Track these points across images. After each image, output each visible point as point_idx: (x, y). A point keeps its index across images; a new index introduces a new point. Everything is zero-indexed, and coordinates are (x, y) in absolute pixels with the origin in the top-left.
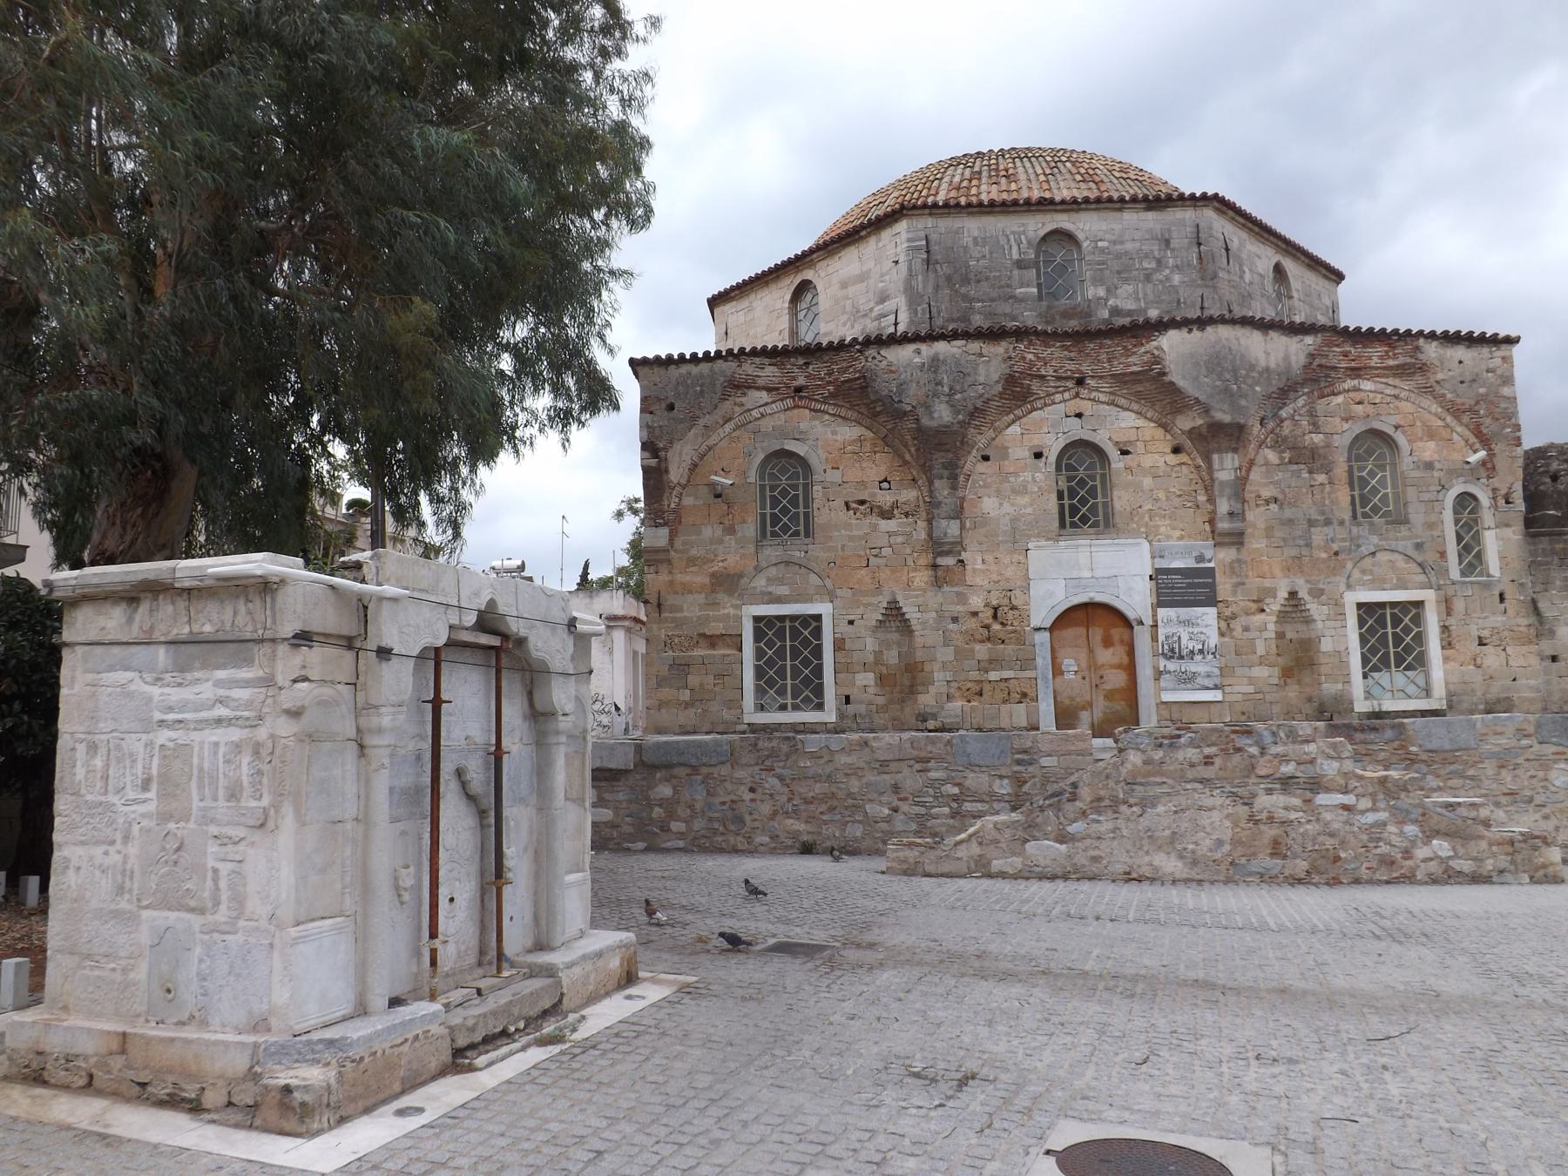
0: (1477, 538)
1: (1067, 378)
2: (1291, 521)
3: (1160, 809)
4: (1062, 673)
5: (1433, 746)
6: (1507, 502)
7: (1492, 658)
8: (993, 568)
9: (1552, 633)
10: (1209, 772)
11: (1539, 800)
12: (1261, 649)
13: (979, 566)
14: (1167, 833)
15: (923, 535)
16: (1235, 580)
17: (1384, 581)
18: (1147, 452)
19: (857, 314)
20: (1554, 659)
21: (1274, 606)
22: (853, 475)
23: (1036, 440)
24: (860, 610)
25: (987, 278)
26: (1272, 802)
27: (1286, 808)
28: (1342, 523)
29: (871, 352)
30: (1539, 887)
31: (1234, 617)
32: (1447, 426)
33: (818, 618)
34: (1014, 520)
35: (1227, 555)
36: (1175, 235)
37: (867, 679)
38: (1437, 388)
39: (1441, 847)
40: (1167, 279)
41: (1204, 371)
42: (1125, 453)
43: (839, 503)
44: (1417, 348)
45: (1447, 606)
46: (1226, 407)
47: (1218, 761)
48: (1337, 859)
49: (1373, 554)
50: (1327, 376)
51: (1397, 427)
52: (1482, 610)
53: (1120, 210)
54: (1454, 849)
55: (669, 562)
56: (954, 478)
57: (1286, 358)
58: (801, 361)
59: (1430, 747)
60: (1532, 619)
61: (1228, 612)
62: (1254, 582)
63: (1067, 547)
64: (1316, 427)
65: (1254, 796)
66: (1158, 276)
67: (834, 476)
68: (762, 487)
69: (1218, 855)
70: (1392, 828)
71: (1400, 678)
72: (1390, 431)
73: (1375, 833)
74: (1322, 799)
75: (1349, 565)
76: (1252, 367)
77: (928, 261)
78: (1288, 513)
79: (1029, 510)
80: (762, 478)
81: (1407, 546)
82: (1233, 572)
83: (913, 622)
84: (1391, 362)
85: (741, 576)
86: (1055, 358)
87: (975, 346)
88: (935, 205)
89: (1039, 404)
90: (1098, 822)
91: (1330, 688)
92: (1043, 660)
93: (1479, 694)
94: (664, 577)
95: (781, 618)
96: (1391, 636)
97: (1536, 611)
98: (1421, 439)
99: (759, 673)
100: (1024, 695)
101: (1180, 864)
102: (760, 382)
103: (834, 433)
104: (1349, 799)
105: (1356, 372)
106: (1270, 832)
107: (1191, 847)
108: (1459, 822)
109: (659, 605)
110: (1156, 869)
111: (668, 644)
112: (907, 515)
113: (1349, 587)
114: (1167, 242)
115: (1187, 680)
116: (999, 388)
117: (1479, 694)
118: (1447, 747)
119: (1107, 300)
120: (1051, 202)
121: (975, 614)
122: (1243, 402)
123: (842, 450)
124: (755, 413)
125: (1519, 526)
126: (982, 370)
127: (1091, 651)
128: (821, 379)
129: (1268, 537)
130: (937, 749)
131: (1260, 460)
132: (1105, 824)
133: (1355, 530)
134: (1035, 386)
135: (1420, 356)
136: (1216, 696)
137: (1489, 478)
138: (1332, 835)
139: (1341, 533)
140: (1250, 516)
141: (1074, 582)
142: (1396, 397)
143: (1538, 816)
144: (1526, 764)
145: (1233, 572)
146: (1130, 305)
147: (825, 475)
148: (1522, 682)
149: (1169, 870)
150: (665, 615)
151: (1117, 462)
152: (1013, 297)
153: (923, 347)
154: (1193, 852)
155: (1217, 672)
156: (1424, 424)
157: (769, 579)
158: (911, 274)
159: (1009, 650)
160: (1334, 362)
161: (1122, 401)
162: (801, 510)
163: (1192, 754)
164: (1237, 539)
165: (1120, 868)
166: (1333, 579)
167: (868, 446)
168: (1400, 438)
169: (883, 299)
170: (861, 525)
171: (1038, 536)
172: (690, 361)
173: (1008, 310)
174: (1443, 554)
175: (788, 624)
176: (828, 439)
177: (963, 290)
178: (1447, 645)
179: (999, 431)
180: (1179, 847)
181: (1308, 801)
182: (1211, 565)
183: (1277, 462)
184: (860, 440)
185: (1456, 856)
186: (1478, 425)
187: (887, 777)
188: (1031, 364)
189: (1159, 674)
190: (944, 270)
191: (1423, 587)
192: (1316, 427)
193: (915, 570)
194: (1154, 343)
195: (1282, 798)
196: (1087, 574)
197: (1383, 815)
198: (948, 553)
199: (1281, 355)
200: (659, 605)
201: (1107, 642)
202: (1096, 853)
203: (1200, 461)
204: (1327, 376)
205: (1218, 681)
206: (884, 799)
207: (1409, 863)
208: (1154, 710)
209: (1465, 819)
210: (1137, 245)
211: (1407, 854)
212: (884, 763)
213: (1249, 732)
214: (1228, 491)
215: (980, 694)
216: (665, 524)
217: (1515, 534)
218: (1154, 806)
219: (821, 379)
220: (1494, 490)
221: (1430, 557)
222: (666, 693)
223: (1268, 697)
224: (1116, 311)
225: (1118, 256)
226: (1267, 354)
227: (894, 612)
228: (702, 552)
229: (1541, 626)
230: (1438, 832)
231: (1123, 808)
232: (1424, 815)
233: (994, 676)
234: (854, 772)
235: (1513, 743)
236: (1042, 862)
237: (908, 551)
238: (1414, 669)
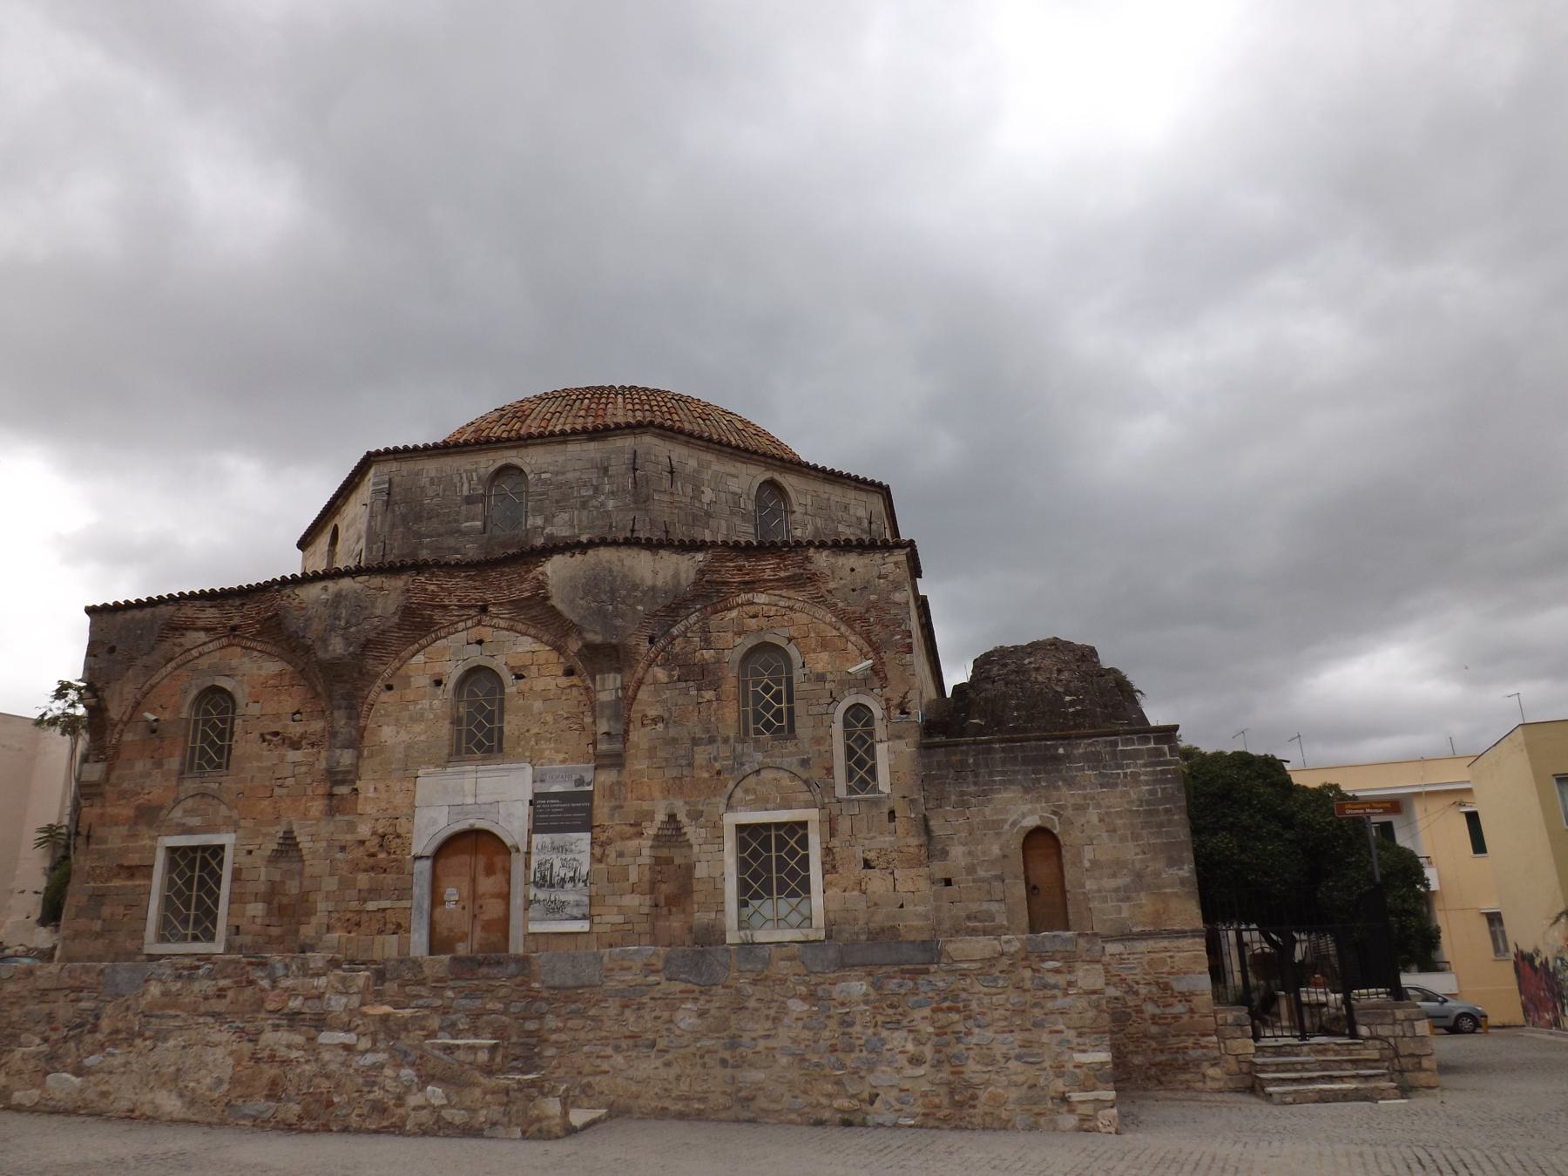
0: (871, 751)
2: (674, 740)
3: (171, 1043)
4: (444, 903)
5: (557, 982)
6: (903, 712)
7: (878, 883)
9: (944, 854)
10: (220, 1006)
11: (662, 1044)
12: (633, 877)
14: (173, 1069)
16: (614, 803)
18: (540, 675)
20: (948, 882)
21: (651, 830)
23: (437, 668)
24: (259, 841)
25: (438, 515)
26: (277, 1039)
27: (289, 1046)
28: (726, 740)
29: (287, 591)
30: (533, 1144)
31: (610, 841)
32: (842, 636)
33: (222, 847)
34: (409, 747)
35: (607, 777)
36: (613, 462)
38: (829, 597)
39: (435, 1094)
40: (602, 504)
41: (581, 594)
42: (519, 677)
43: (256, 734)
44: (808, 559)
47: (230, 994)
48: (330, 1104)
49: (758, 772)
50: (718, 591)
52: (869, 830)
53: (565, 442)
54: (447, 1097)
55: (101, 795)
57: (676, 576)
58: (238, 603)
59: (551, 983)
60: (923, 839)
61: (603, 837)
62: (632, 805)
63: (454, 773)
64: (707, 643)
65: (260, 1032)
69: (216, 1095)
70: (388, 1072)
71: (784, 905)
72: (782, 643)
73: (371, 1077)
74: (326, 1037)
75: (731, 785)
76: (635, 587)
77: (387, 503)
78: (672, 732)
79: (423, 738)
81: (792, 762)
82: (612, 795)
83: (305, 852)
84: (783, 574)
85: (161, 808)
86: (459, 588)
87: (377, 581)
88: (552, 434)
90: (113, 1055)
91: (702, 917)
92: (421, 890)
93: (861, 922)
94: (97, 810)
96: (771, 860)
97: (927, 830)
98: (814, 651)
99: (167, 903)
100: (399, 926)
101: (179, 1103)
102: (200, 623)
103: (260, 668)
104: (350, 1038)
105: (750, 586)
106: (271, 1071)
107: (192, 1084)
108: (456, 1066)
109: (88, 837)
110: (157, 1107)
112: (313, 745)
114: (606, 470)
115: (555, 909)
116: (396, 619)
117: (861, 922)
118: (570, 983)
120: (607, 428)
121: (362, 842)
122: (619, 622)
124: (195, 653)
125: (914, 737)
126: (380, 603)
127: (474, 880)
129: (651, 758)
130: (89, 979)
131: (649, 678)
132: (119, 1057)
133: (739, 747)
134: (437, 615)
135: (809, 566)
136: (583, 926)
137: (882, 688)
138: (327, 1077)
139: (725, 751)
140: (634, 736)
141: (458, 809)
142: (791, 609)
143: (658, 1063)
144: (652, 1004)
145: (612, 795)
147: (248, 708)
148: (909, 908)
149: (169, 1109)
150: (92, 846)
152: (459, 531)
154: (193, 1090)
155: (586, 900)
157: (185, 811)
159: (389, 879)
160: (727, 577)
161: (520, 627)
163: (207, 986)
164: (616, 761)
165: (124, 1104)
166: (713, 800)
168: (793, 651)
171: (429, 763)
174: (829, 771)
175: (199, 855)
176: (251, 673)
177: (415, 527)
178: (829, 868)
180: (181, 1085)
181: (311, 1039)
182: (590, 788)
184: (281, 674)
185: (449, 1105)
186: (869, 633)
187: (43, 1006)
188: (434, 595)
189: (528, 903)
190: (400, 509)
191: (808, 805)
192: (707, 643)
193: (313, 799)
195: (286, 1035)
196: (470, 800)
197: (382, 1057)
198: (343, 782)
199: (671, 573)
200: (88, 837)
201: (490, 871)
202: (104, 1088)
204: (718, 591)
205: (586, 910)
206: (39, 1028)
207: (401, 1111)
208: (521, 941)
209: (462, 1064)
210: (577, 474)
211: (400, 1100)
212: (45, 992)
213: (263, 964)
214: (607, 712)
215: (358, 924)
217: (907, 748)
218: (165, 1040)
220: (888, 700)
221: (816, 773)
223: (637, 928)
224: (551, 537)
225: (559, 486)
226: (656, 573)
227: (289, 845)
229: (932, 849)
230: (433, 1077)
231: (138, 1041)
232: (421, 1057)
233: (371, 906)
234: (18, 1000)
235: (640, 979)
236: (58, 1095)
238: (761, 897)
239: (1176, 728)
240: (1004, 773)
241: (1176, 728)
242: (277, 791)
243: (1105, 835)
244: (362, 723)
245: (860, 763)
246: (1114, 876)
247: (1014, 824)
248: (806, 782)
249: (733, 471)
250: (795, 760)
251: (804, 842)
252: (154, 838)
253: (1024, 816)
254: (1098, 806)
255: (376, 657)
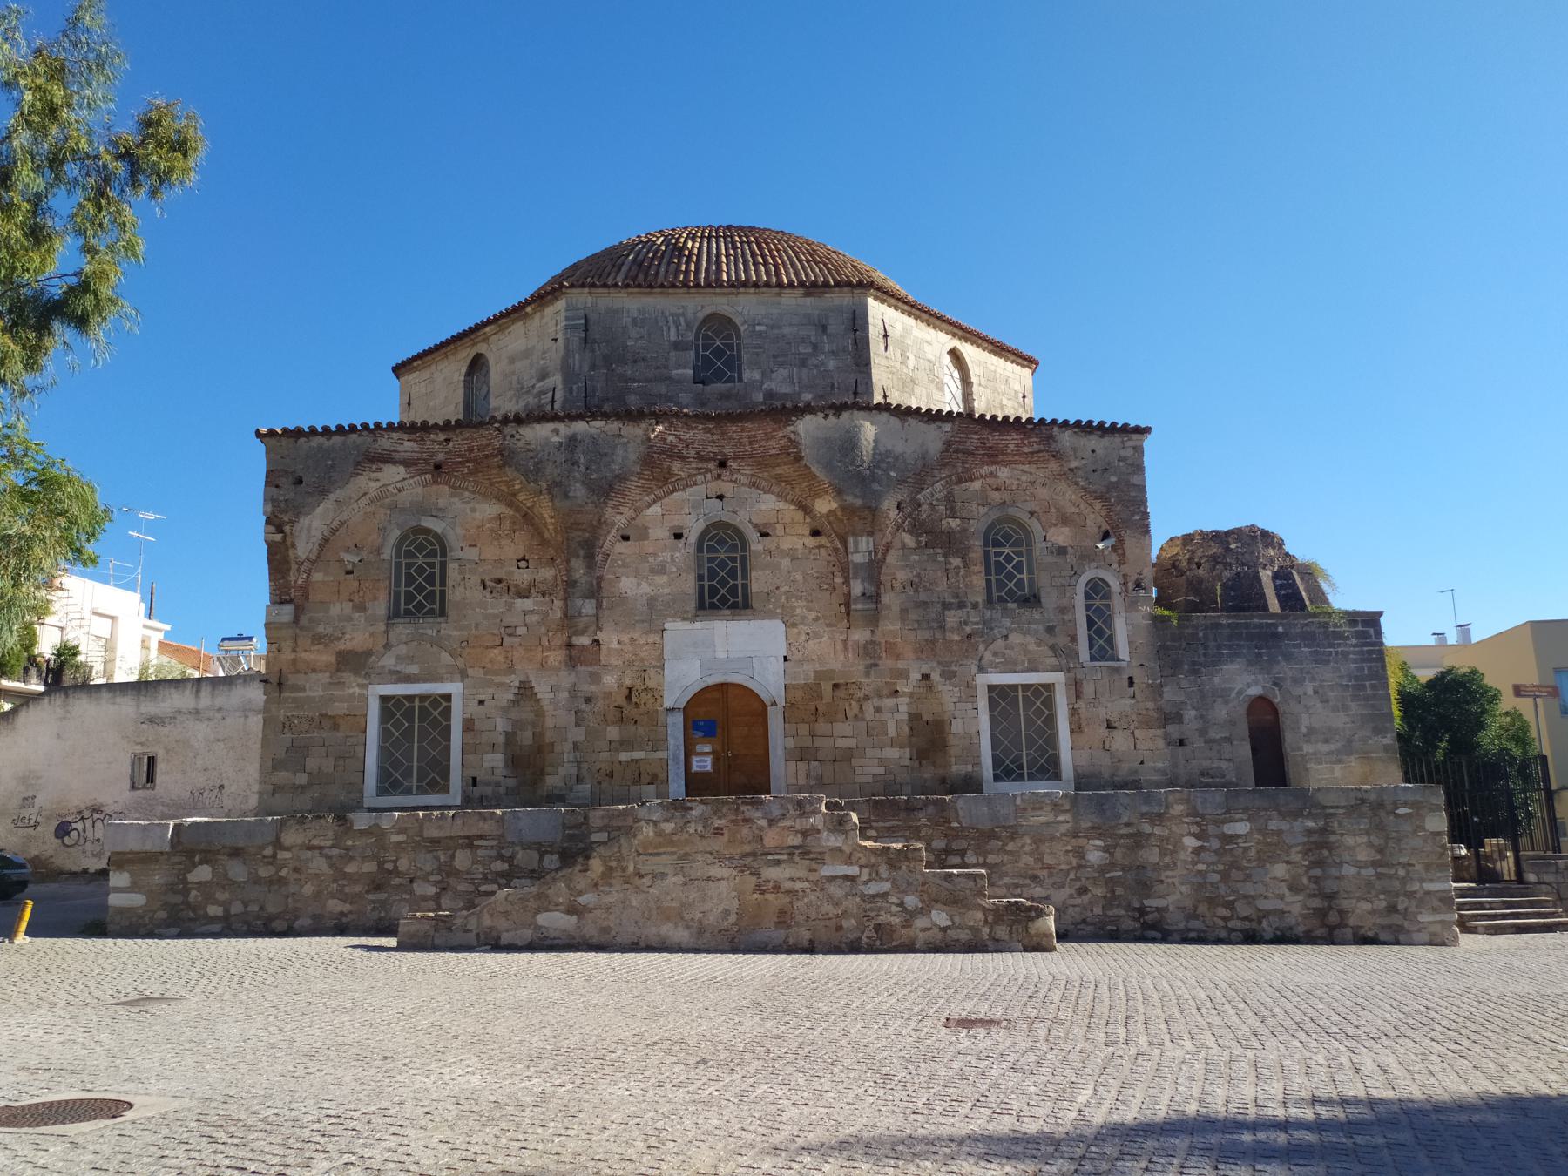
0: (1109, 622)
1: (708, 460)
2: (925, 604)
7: (1120, 742)
8: (628, 648)
13: (615, 645)
15: (559, 614)
17: (1015, 663)
19: (522, 390)
22: (490, 553)
23: (676, 521)
28: (975, 606)
29: (509, 429)
33: (448, 697)
37: (496, 760)
42: (764, 535)
43: (476, 580)
44: (1051, 437)
45: (1076, 688)
46: (857, 491)
51: (1032, 514)
54: (951, 918)
56: (590, 558)
66: (812, 361)
67: (472, 554)
68: (398, 565)
72: (1024, 517)
75: (982, 648)
78: (923, 596)
79: (666, 591)
80: (398, 555)
82: (867, 654)
83: (545, 703)
84: (1026, 450)
89: (680, 484)
95: (410, 698)
103: (473, 510)
109: (280, 684)
111: (286, 725)
113: (981, 670)
114: (824, 328)
119: (762, 383)
122: (876, 486)
123: (481, 528)
128: (461, 456)
133: (988, 614)
139: (974, 617)
145: (867, 654)
146: (785, 389)
147: (461, 551)
151: (757, 545)
152: (669, 378)
153: (561, 427)
156: (1058, 510)
157: (398, 658)
158: (568, 352)
162: (437, 588)
167: (507, 525)
168: (1035, 525)
169: (543, 376)
170: (497, 606)
171: (674, 617)
172: (322, 434)
173: (664, 391)
174: (1074, 639)
177: (620, 370)
179: (638, 511)
183: (913, 545)
184: (500, 518)
193: (549, 649)
194: (791, 428)
200: (280, 684)
203: (837, 544)
216: (290, 601)
219: (461, 456)
221: (1062, 640)
222: (282, 776)
224: (770, 395)
228: (330, 630)
233: (624, 756)
235: (1051, 818)
237: (543, 630)
239: (1380, 613)
240: (1230, 647)
241: (1380, 613)
242: (507, 640)
243: (1319, 705)
244: (598, 574)
245: (1100, 633)
246: (1326, 741)
247: (1240, 693)
248: (1052, 648)
249: (928, 338)
250: (1041, 627)
251: (1049, 703)
252: (365, 686)
253: (1249, 685)
254: (1313, 679)
255: (615, 507)
